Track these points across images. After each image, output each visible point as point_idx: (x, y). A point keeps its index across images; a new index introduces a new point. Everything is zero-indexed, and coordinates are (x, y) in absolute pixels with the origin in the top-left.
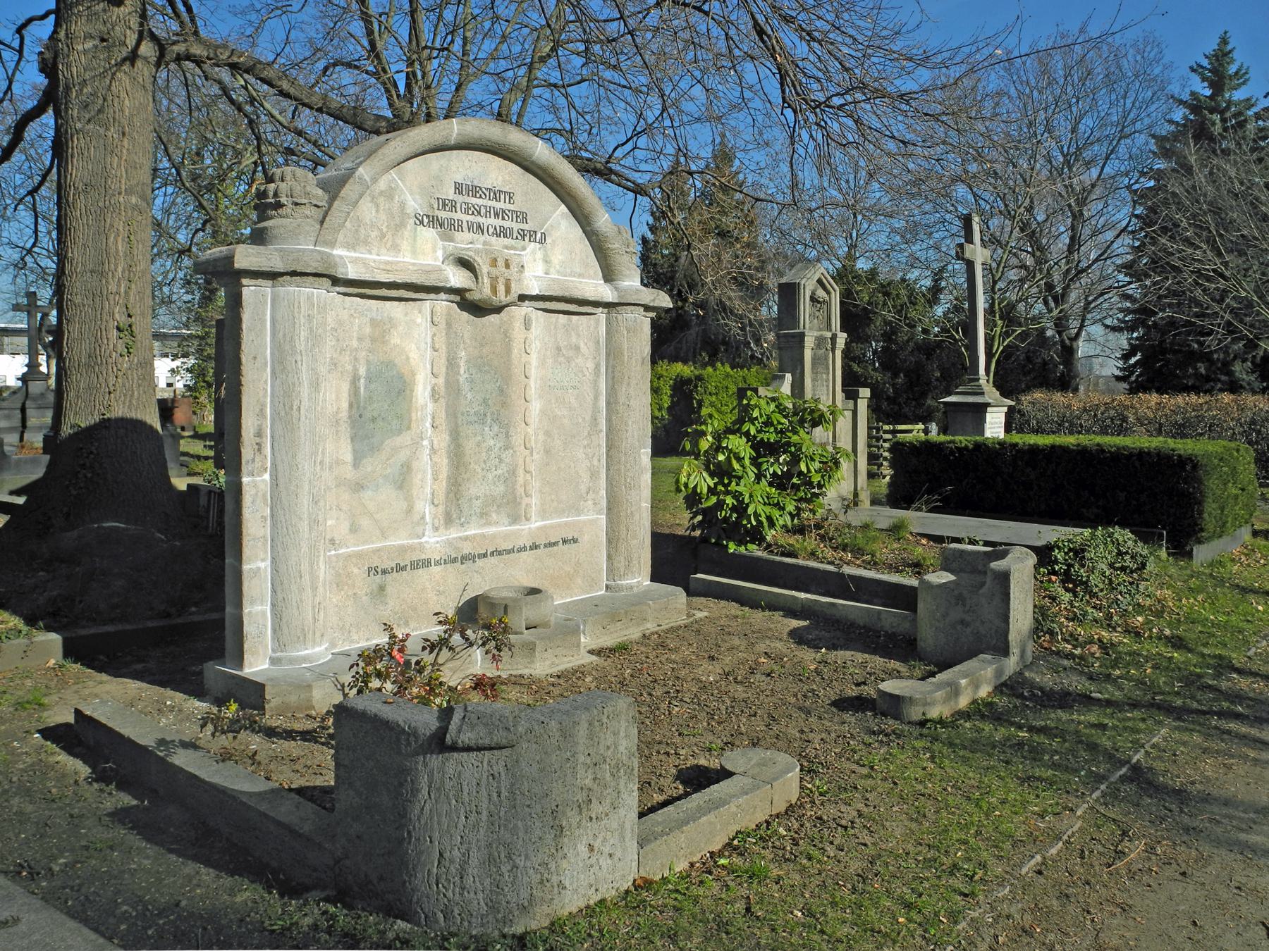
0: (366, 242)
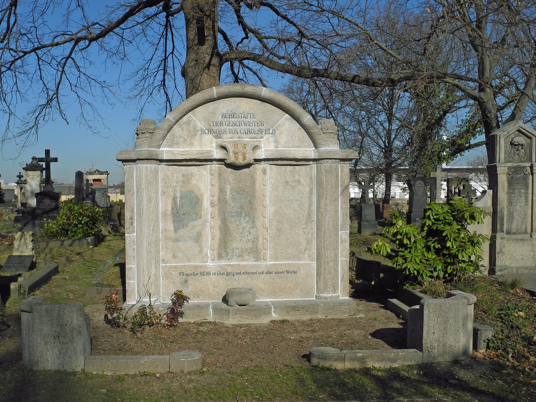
0: (177, 144)
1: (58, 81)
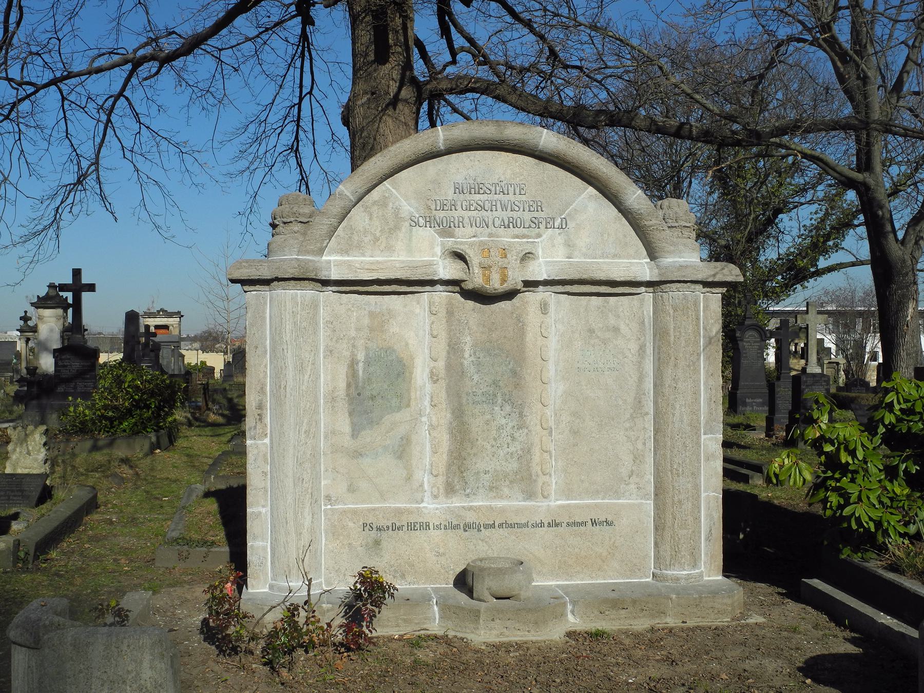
1: (98, 140)
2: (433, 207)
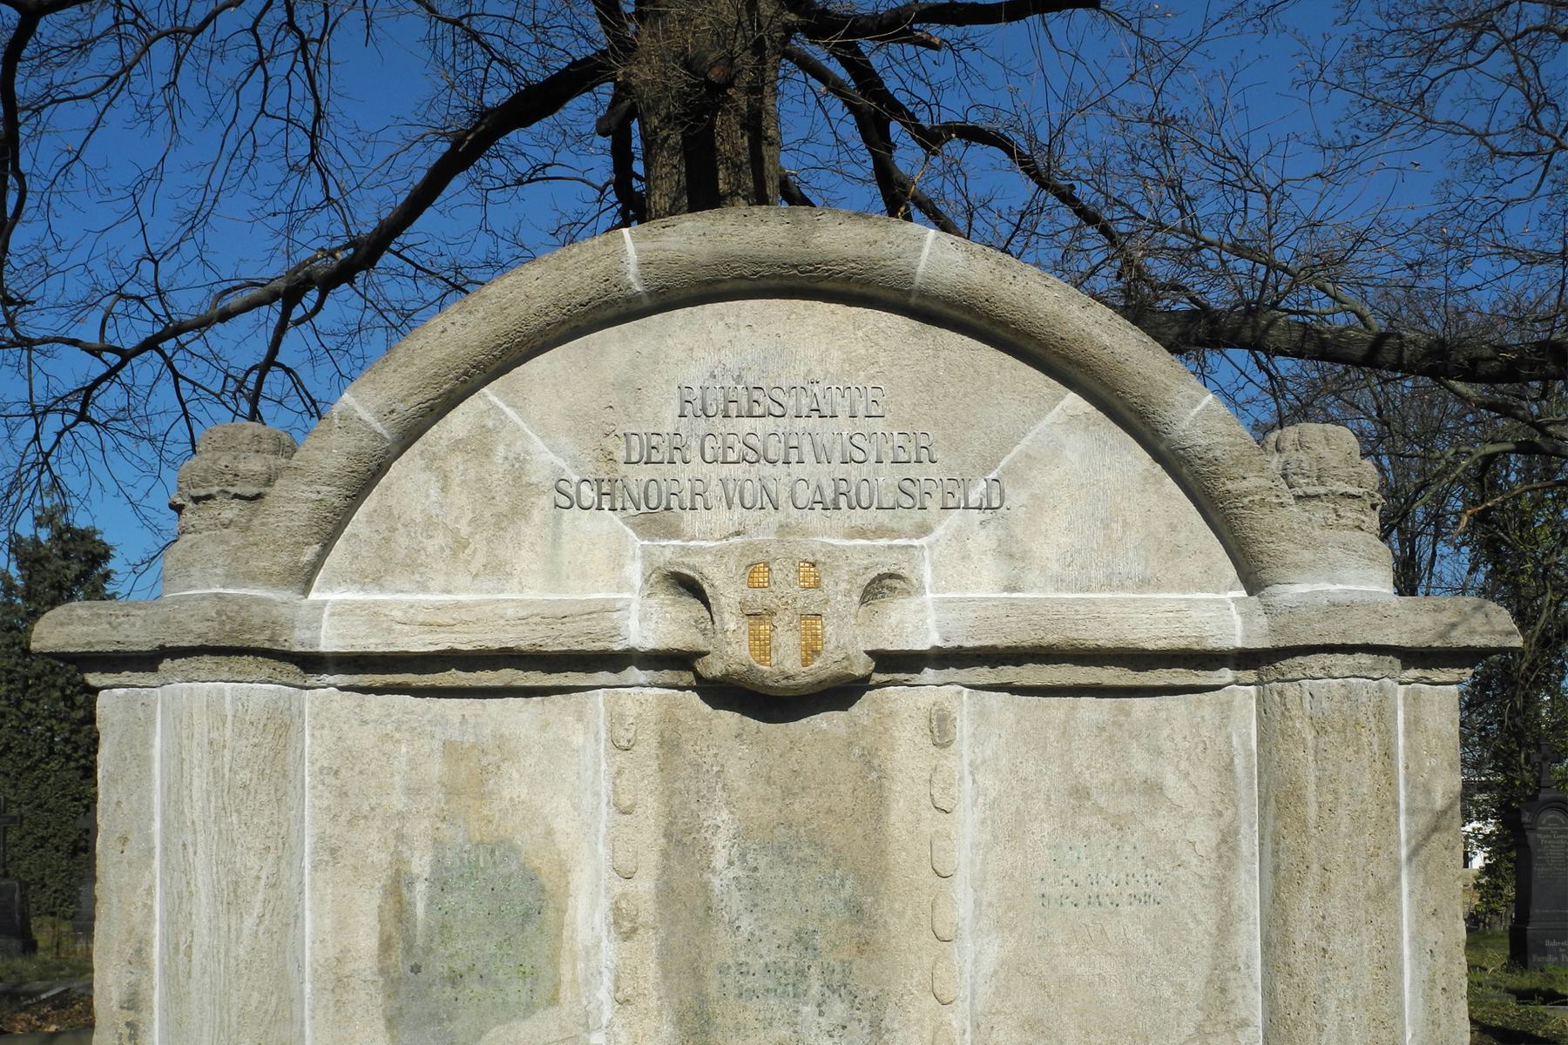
0: (412, 565)
2: (620, 455)
